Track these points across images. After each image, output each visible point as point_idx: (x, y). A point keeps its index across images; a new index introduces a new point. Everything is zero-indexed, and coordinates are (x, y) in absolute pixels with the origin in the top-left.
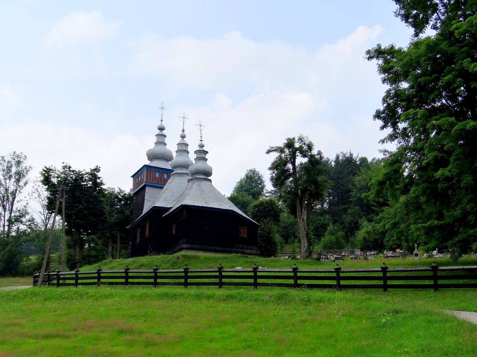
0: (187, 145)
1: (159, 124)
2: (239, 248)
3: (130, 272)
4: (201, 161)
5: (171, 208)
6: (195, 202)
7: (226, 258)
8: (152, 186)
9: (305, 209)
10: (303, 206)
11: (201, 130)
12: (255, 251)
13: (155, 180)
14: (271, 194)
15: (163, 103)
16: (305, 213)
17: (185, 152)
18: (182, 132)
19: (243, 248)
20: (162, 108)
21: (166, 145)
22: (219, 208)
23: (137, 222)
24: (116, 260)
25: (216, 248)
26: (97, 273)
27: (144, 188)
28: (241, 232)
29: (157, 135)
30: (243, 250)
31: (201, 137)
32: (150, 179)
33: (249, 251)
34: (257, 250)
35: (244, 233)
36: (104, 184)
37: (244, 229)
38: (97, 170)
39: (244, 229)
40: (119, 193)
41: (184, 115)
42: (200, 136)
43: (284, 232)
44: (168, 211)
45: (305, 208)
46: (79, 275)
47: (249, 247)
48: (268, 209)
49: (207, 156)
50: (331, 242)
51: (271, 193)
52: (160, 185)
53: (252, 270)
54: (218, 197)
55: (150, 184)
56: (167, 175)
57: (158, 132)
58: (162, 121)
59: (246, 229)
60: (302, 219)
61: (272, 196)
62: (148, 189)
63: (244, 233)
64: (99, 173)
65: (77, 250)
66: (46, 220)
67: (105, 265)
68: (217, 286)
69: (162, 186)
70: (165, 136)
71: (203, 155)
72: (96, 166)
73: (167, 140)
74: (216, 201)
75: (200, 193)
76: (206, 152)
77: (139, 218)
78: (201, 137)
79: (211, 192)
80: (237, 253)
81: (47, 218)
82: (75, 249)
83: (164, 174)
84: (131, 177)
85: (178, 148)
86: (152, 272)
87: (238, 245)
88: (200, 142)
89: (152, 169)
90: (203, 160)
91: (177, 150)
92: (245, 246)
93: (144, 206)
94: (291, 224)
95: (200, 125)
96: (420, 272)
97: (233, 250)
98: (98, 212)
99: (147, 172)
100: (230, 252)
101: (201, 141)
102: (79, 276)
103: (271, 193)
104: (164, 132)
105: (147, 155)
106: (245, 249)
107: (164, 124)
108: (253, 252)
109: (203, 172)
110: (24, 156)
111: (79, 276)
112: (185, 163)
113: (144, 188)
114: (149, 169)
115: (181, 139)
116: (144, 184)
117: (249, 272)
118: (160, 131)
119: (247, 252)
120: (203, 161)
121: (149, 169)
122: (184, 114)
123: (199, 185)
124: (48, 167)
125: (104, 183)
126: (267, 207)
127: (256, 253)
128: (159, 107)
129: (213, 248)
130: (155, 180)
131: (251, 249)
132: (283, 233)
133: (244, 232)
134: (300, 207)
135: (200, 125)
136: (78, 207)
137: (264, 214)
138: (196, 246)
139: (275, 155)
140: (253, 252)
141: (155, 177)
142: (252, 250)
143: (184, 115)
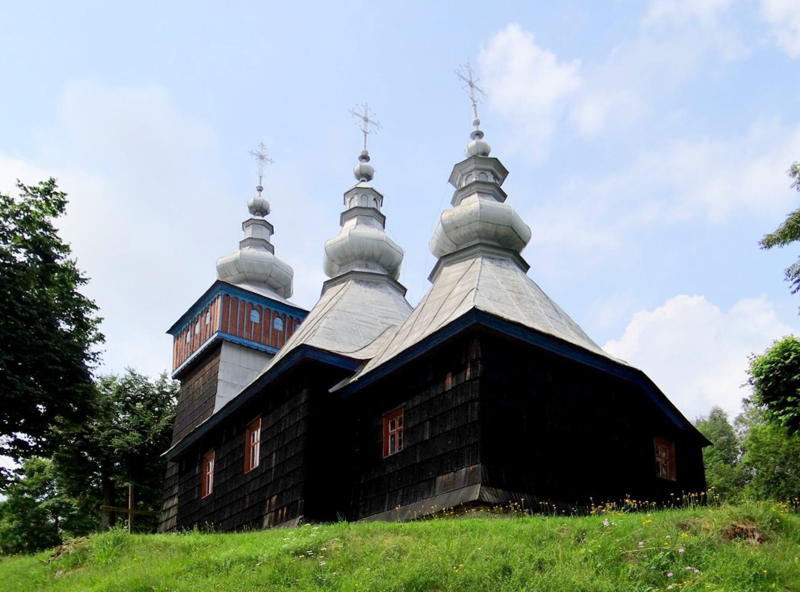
0: (379, 197)
1: (252, 197)
5: (365, 362)
8: (241, 346)
13: (249, 330)
23: (205, 429)
24: (159, 538)
27: (213, 350)
32: (234, 325)
36: (83, 280)
40: (129, 382)
44: (352, 374)
52: (264, 347)
56: (284, 322)
62: (226, 353)
64: (61, 216)
67: (75, 565)
69: (269, 349)
72: (47, 180)
77: (203, 422)
83: (274, 319)
84: (169, 332)
93: (217, 398)
98: (55, 362)
101: (479, 134)
105: (218, 269)
107: (265, 197)
113: (213, 350)
114: (231, 296)
116: (216, 335)
130: (249, 330)
141: (250, 322)
143: (366, 111)
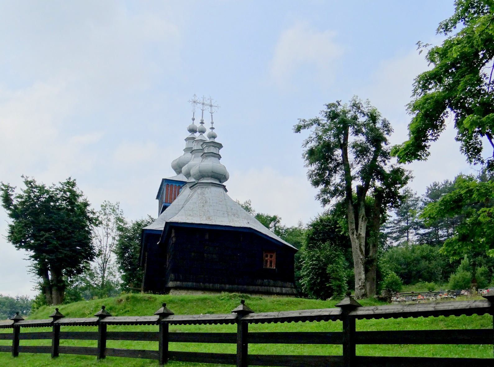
1: (189, 123)
2: (262, 285)
3: (251, 321)
4: (209, 159)
6: (190, 218)
7: (204, 300)
9: (362, 219)
10: (360, 214)
11: (212, 113)
12: (287, 289)
14: (393, 224)
15: (195, 95)
16: (363, 225)
17: (214, 157)
18: (200, 124)
20: (194, 102)
21: (219, 157)
22: (229, 225)
26: (157, 322)
28: (267, 261)
29: (186, 140)
31: (212, 123)
33: (278, 290)
34: (292, 288)
35: (271, 262)
37: (271, 257)
38: (71, 184)
39: (271, 257)
42: (211, 121)
43: (404, 269)
45: (363, 217)
46: (61, 327)
47: (280, 283)
48: (329, 229)
49: (221, 152)
50: (464, 279)
51: (393, 223)
53: (232, 316)
54: (232, 209)
57: (189, 135)
59: (274, 255)
60: (356, 235)
61: (394, 226)
63: (271, 262)
65: (53, 296)
66: (103, 264)
68: (49, 355)
71: (213, 150)
74: (226, 215)
75: (202, 204)
76: (220, 146)
78: (212, 123)
79: (220, 203)
80: (231, 291)
81: (104, 262)
82: (51, 293)
86: (232, 321)
87: (259, 281)
89: (174, 184)
90: (212, 156)
92: (272, 282)
94: (414, 260)
95: (211, 106)
96: (69, 327)
97: (251, 288)
99: (167, 189)
100: (219, 291)
101: (212, 128)
102: (23, 330)
103: (393, 223)
106: (272, 286)
108: (284, 290)
109: (210, 175)
110: (80, 191)
111: (23, 330)
112: (176, 162)
114: (170, 184)
115: (200, 134)
117: (327, 318)
118: (191, 134)
119: (275, 291)
120: (213, 158)
121: (170, 184)
123: (202, 194)
124: (6, 184)
125: (89, 203)
126: (328, 226)
127: (290, 292)
128: (189, 101)
131: (282, 287)
132: (403, 271)
133: (271, 262)
134: (353, 216)
136: (44, 235)
137: (324, 235)
139: (309, 133)
140: (284, 290)
142: (283, 289)
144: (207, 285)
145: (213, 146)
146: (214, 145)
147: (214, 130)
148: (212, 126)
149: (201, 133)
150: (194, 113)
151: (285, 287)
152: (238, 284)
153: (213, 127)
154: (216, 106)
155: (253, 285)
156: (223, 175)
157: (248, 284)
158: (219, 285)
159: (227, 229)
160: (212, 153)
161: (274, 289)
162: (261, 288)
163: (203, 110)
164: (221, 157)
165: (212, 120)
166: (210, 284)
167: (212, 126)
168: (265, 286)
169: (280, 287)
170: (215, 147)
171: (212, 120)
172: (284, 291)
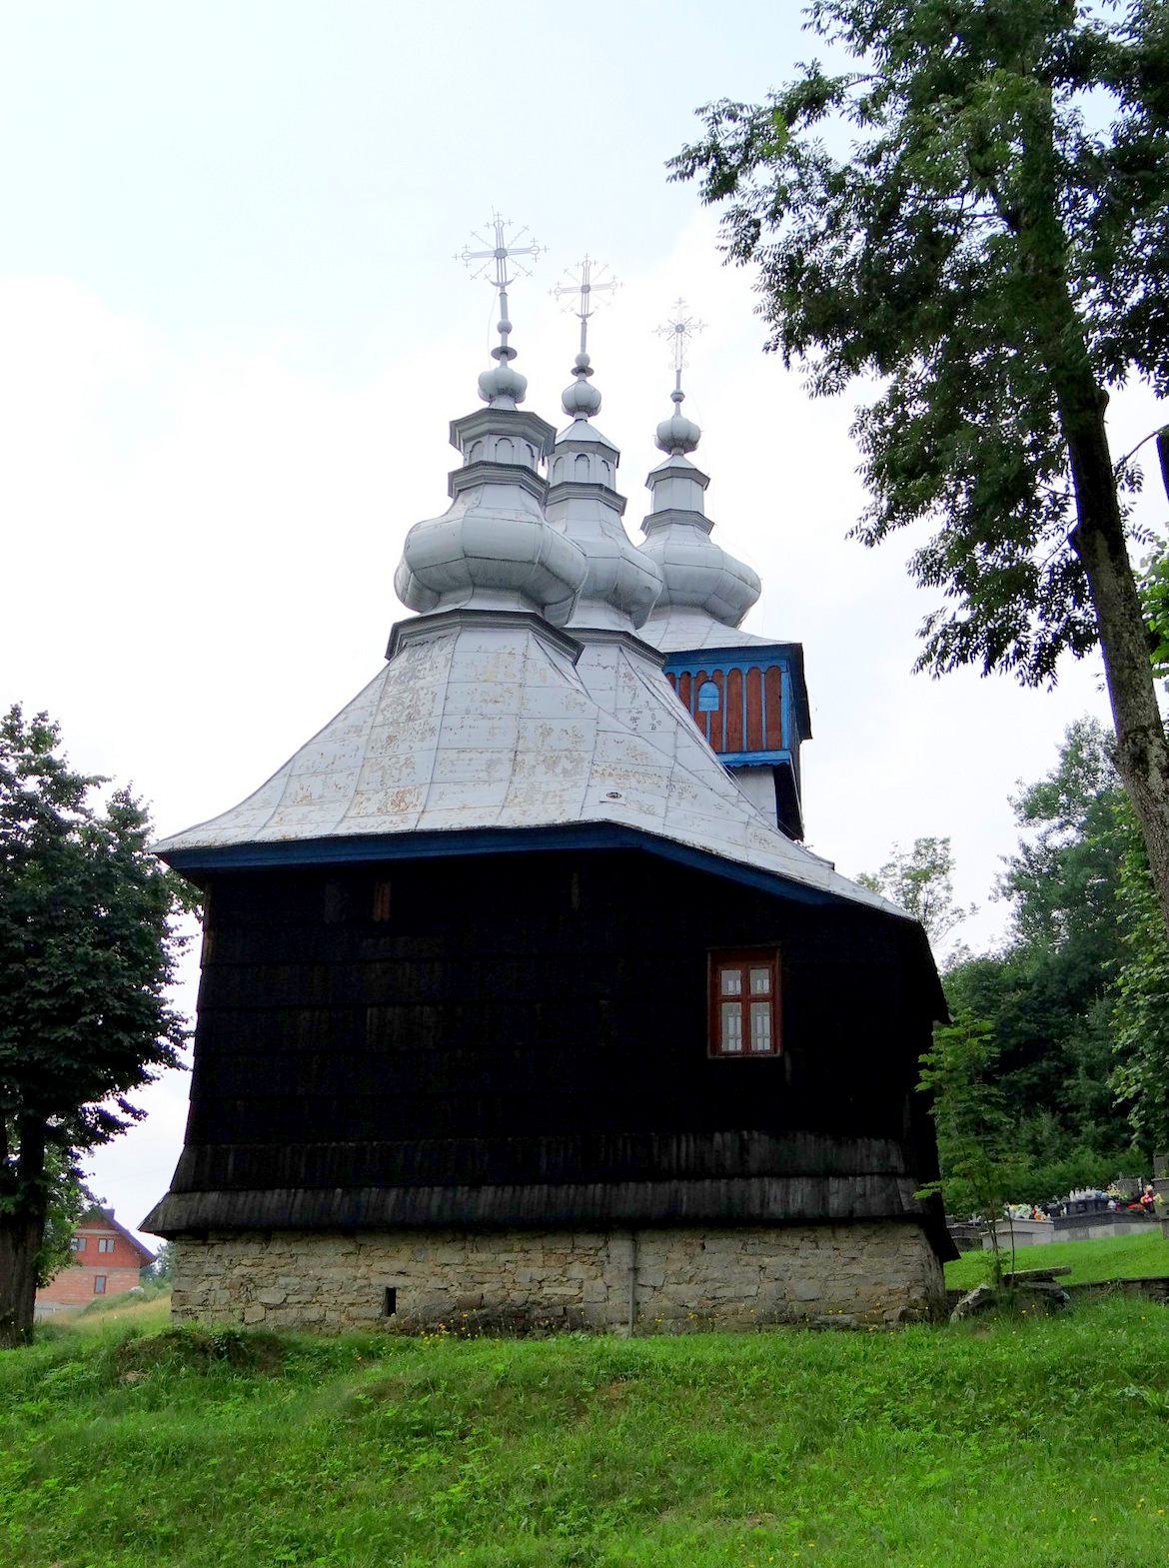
1: (665, 412)
2: (696, 1172)
12: (859, 1185)
17: (502, 482)
18: (575, 379)
19: (746, 1176)
20: (680, 329)
21: (707, 526)
25: (462, 1193)
30: (738, 1185)
33: (799, 1195)
34: (889, 1174)
35: (747, 1017)
41: (499, 235)
42: (497, 319)
47: (809, 1148)
55: (750, 757)
56: (720, 688)
57: (661, 459)
58: (678, 398)
70: (702, 480)
73: (712, 504)
79: (489, 708)
85: (655, 502)
87: (684, 1148)
88: (496, 363)
91: (649, 512)
92: (761, 1146)
97: (632, 1197)
104: (692, 459)
107: (692, 413)
108: (838, 1196)
119: (776, 1209)
122: (586, 267)
127: (877, 1205)
128: (659, 331)
129: (432, 1200)
135: (500, 254)
138: (273, 1199)
140: (838, 1196)
142: (834, 1184)
143: (499, 235)
144: (370, 1195)
145: (491, 433)
146: (501, 426)
147: (512, 364)
148: (504, 339)
149: (580, 415)
150: (679, 372)
151: (842, 1174)
152: (555, 1179)
153: (510, 344)
154: (526, 251)
155: (640, 1177)
156: (531, 562)
157: (614, 1176)
158: (545, 1187)
159: (482, 848)
160: (600, 485)
161: (775, 1189)
162: (690, 1195)
163: (584, 317)
164: (624, 500)
165: (583, 345)
166: (387, 1188)
167: (504, 339)
168: (715, 1177)
169: (810, 1175)
170: (505, 435)
171: (583, 345)
172: (836, 1203)
